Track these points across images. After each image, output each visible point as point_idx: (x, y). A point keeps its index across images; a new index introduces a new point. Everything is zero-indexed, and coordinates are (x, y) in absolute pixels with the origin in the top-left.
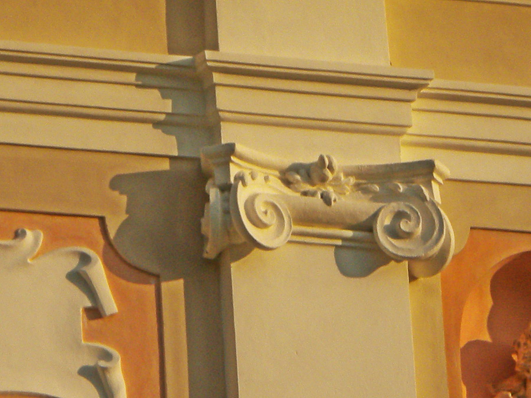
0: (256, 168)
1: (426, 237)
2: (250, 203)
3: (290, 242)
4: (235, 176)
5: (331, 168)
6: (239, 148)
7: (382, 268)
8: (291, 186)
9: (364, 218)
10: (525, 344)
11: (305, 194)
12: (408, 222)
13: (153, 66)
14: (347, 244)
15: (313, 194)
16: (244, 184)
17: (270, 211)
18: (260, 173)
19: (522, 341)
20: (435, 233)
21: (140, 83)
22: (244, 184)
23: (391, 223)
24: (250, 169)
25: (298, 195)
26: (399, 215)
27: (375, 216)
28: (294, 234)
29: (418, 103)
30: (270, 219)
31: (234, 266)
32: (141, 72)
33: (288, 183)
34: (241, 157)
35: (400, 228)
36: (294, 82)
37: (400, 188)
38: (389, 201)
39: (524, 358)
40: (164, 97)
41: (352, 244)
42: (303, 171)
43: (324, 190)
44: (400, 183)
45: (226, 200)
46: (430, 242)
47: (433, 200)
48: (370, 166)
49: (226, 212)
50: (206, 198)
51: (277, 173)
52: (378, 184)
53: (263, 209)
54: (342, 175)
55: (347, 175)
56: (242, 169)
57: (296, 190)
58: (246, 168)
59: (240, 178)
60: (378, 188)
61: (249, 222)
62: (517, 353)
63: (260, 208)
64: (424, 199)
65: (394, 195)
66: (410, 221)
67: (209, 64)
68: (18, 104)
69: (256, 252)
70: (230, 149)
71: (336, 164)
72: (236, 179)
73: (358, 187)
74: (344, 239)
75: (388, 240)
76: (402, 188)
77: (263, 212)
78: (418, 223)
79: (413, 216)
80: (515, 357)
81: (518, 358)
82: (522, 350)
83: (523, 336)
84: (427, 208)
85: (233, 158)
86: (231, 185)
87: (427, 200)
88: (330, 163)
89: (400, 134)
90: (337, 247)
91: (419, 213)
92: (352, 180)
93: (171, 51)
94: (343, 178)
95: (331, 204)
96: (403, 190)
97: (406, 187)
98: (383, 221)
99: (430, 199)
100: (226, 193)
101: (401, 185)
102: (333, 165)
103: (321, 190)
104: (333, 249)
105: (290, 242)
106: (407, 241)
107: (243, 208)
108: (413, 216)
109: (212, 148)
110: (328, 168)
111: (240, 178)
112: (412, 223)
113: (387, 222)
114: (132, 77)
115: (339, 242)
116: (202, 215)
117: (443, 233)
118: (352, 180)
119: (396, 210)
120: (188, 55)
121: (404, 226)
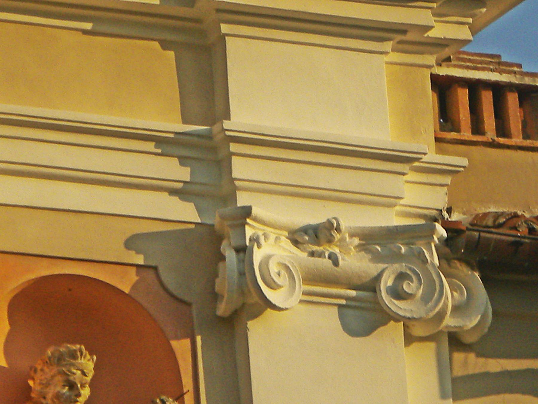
0: (269, 230)
1: (426, 299)
3: (301, 301)
4: (250, 237)
5: (338, 229)
6: (255, 211)
7: (382, 328)
8: (300, 246)
9: (366, 279)
10: (42, 370)
11: (312, 254)
12: (410, 283)
13: (172, 136)
14: (353, 303)
15: (321, 255)
16: (259, 247)
17: (283, 272)
19: (39, 367)
20: (436, 295)
21: (159, 151)
22: (259, 247)
23: (392, 284)
24: (264, 230)
25: (305, 255)
26: (401, 277)
28: (305, 293)
29: (412, 176)
30: (282, 280)
31: (250, 324)
32: (159, 141)
33: (296, 243)
34: (255, 220)
35: (403, 289)
36: (89, 136)
38: (393, 263)
39: (40, 384)
40: (182, 164)
41: (353, 303)
42: (311, 232)
43: (331, 250)
44: (402, 244)
45: (241, 261)
46: (430, 304)
47: (433, 262)
48: (375, 227)
49: (242, 274)
50: (222, 258)
51: (286, 234)
52: (379, 244)
53: (276, 271)
54: (347, 235)
55: (352, 236)
56: (257, 231)
57: (303, 250)
58: (259, 229)
59: (255, 240)
61: (263, 283)
62: (33, 379)
63: (274, 268)
64: (425, 261)
65: (397, 257)
66: (412, 282)
67: (228, 133)
68: (113, 176)
69: (269, 311)
70: (247, 212)
71: (343, 225)
73: (361, 248)
74: (347, 298)
77: (277, 273)
78: (421, 285)
79: (414, 277)
80: (31, 383)
81: (34, 384)
82: (39, 376)
83: (39, 362)
84: (427, 268)
85: (248, 220)
88: (338, 224)
89: (391, 206)
90: (340, 306)
91: (421, 275)
92: (229, 223)
93: (185, 121)
94: (348, 239)
95: (338, 264)
96: (405, 251)
97: (407, 248)
98: (386, 283)
99: (431, 261)
100: (241, 255)
101: (403, 247)
102: (341, 227)
103: (328, 250)
104: (336, 309)
105: (301, 301)
106: (409, 301)
107: (258, 267)
109: (228, 210)
110: (336, 230)
111: (255, 240)
112: (414, 285)
113: (390, 283)
114: (150, 146)
115: (343, 302)
116: (217, 276)
117: (443, 295)
118: (356, 241)
119: (399, 271)
120: (206, 126)
121: (407, 287)
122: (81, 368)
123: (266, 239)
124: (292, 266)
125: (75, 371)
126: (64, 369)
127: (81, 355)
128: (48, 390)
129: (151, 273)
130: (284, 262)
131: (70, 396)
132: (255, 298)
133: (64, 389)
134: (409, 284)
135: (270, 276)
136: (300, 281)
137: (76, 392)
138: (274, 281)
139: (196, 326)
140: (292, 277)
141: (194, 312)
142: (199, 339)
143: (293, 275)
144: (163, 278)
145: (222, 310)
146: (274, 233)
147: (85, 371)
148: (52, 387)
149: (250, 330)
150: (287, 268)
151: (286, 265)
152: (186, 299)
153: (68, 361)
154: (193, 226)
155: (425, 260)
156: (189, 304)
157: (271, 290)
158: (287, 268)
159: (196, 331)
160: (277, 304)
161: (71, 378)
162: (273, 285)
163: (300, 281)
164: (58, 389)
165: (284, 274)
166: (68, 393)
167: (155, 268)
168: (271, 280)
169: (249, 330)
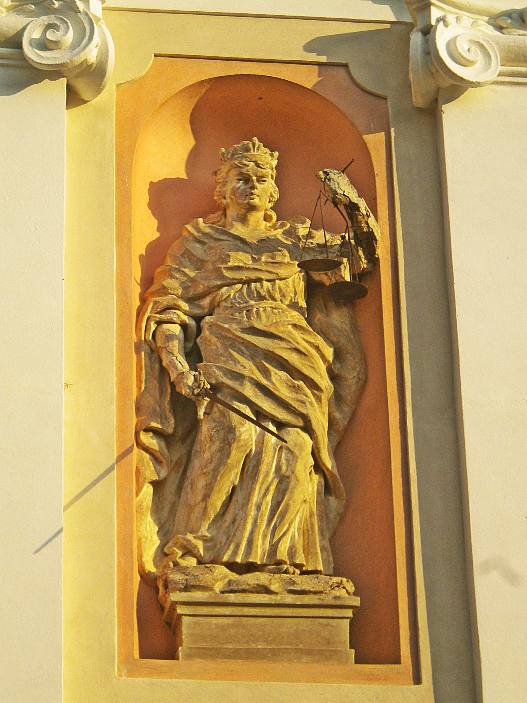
2: (451, 47)
8: (504, 31)
9: (12, 32)
12: (55, 31)
16: (446, 25)
17: (474, 48)
18: (467, 18)
22: (446, 25)
24: (457, 14)
27: (24, 29)
33: (500, 29)
37: (54, 4)
60: (33, 7)
63: (462, 47)
72: (438, 21)
75: (36, 53)
76: (57, 4)
86: (432, 26)
87: (80, 12)
98: (30, 34)
108: (58, 22)
121: (50, 36)
122: (254, 160)
123: (458, 21)
124: (490, 47)
125: (247, 163)
126: (236, 162)
127: (254, 147)
128: (226, 188)
129: (342, 72)
130: (477, 40)
131: (246, 189)
132: (446, 82)
133: (239, 183)
134: (54, 32)
135: (458, 51)
136: (497, 57)
137: (250, 185)
138: (462, 56)
139: (391, 119)
140: (487, 55)
141: (389, 104)
142: (392, 130)
143: (489, 53)
144: (353, 73)
145: (419, 101)
146: (472, 18)
147: (259, 162)
148: (229, 184)
149: (445, 112)
150: (481, 46)
151: (479, 42)
152: (380, 92)
153: (240, 154)
154: (388, 26)
155: (76, 10)
156: (385, 98)
157: (466, 67)
158: (481, 46)
159: (391, 125)
160: (464, 77)
161: (244, 170)
162: (464, 62)
163: (497, 57)
164: (234, 184)
165: (476, 50)
166: (243, 187)
167: (346, 66)
168: (459, 55)
169: (444, 113)
